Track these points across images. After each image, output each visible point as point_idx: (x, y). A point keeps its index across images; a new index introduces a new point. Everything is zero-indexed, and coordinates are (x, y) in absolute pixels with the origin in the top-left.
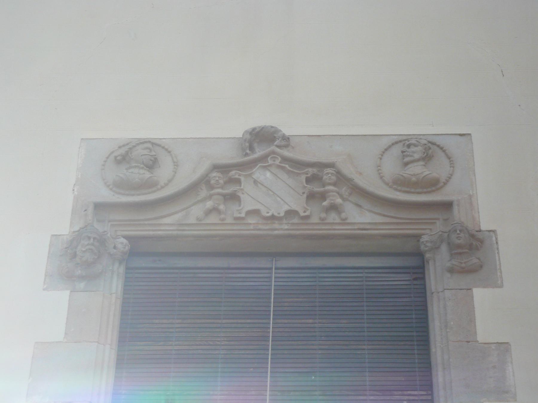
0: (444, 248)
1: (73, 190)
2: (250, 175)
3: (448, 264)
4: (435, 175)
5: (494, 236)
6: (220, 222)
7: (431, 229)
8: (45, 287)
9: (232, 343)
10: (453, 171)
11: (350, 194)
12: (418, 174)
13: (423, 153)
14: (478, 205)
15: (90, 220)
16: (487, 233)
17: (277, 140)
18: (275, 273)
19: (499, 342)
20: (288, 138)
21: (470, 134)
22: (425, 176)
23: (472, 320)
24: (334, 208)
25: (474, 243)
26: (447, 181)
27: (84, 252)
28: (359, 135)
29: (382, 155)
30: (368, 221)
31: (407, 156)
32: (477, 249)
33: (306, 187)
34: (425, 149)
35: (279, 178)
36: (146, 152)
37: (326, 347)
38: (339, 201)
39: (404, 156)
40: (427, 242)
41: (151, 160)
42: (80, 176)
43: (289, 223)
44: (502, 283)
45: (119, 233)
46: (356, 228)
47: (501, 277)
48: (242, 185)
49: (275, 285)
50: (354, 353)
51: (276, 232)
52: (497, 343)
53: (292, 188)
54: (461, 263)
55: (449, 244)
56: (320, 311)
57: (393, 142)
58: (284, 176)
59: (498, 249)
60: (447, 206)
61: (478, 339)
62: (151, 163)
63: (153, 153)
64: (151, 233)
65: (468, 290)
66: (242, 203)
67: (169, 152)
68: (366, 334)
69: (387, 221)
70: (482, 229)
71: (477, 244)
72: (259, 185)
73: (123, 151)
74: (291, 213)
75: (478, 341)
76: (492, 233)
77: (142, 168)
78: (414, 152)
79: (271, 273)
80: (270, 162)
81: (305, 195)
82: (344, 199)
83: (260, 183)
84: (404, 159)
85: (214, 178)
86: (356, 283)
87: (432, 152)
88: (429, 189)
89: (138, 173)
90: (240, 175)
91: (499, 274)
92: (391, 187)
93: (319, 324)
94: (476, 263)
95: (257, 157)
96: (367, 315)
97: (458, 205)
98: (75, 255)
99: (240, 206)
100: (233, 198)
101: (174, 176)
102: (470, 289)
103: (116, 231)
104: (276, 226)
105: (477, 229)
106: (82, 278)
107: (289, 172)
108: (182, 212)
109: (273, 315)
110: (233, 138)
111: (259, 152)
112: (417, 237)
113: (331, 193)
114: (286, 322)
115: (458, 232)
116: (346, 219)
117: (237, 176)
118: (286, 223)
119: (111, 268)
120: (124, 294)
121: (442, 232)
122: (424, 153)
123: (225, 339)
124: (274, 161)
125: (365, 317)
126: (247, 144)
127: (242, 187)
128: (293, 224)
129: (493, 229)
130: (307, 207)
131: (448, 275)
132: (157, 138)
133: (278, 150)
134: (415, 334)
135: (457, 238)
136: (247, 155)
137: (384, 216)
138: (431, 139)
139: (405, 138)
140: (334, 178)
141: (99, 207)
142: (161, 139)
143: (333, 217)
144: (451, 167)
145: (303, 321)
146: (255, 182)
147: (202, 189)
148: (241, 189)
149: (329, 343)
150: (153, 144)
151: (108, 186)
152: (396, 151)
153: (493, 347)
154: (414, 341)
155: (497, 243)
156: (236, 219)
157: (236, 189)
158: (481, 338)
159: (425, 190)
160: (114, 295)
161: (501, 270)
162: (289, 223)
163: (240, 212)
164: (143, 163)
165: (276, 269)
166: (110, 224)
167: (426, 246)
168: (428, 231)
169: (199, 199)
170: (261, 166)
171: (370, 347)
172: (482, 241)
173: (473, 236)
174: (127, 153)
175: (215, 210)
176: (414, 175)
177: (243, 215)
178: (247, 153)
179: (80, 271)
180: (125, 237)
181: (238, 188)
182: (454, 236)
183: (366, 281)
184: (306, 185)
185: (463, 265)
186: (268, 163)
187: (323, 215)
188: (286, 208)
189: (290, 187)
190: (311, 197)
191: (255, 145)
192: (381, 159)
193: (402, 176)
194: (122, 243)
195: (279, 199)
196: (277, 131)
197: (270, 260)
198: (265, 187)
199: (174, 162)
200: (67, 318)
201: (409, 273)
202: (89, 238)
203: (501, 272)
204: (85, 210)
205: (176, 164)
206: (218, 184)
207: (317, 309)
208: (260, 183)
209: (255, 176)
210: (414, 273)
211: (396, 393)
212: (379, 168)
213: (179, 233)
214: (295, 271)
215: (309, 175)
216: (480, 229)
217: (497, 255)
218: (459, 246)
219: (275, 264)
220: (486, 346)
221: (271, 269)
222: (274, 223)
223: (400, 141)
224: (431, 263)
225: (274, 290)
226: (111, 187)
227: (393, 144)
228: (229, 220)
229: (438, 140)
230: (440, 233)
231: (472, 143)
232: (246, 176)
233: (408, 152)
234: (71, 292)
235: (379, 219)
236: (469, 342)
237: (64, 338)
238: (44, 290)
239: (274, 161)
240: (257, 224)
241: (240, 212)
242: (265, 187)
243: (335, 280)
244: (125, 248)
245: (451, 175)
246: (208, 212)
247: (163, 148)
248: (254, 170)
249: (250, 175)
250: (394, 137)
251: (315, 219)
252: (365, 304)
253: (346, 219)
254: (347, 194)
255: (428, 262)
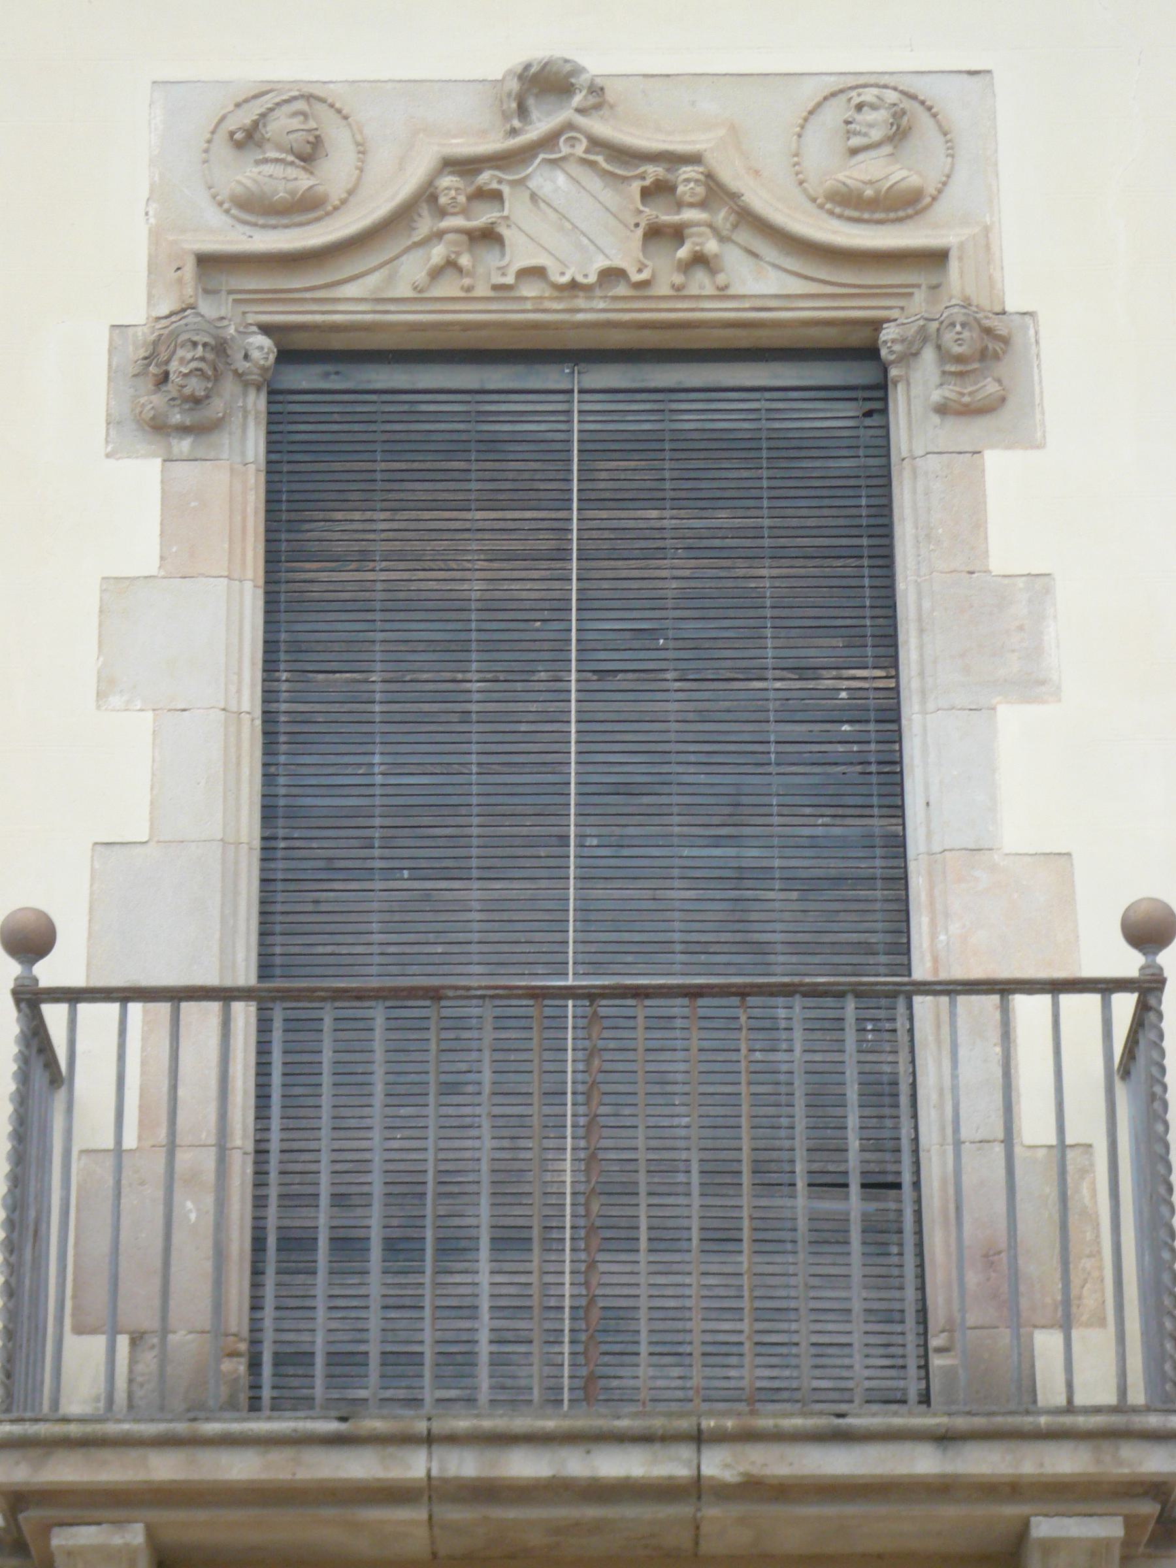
0: (929, 355)
1: (147, 214)
2: (521, 182)
3: (936, 396)
4: (914, 180)
5: (1032, 326)
6: (463, 294)
7: (902, 308)
8: (109, 449)
9: (496, 565)
10: (953, 165)
11: (735, 226)
12: (877, 181)
13: (889, 126)
14: (1001, 249)
15: (191, 297)
16: (1017, 317)
17: (577, 91)
18: (579, 402)
19: (1034, 572)
20: (602, 89)
21: (989, 72)
22: (891, 187)
23: (979, 525)
24: (700, 260)
25: (990, 346)
26: (940, 191)
27: (185, 375)
28: (752, 75)
29: (802, 127)
30: (773, 290)
31: (856, 133)
32: (997, 357)
33: (641, 212)
34: (894, 115)
35: (584, 188)
36: (296, 123)
37: (687, 573)
38: (711, 246)
39: (848, 132)
40: (894, 341)
41: (308, 142)
42: (157, 178)
43: (606, 297)
44: (1044, 436)
45: (251, 318)
46: (747, 305)
47: (1043, 424)
48: (507, 205)
49: (580, 431)
50: (820, 1370)
51: (580, 317)
52: (1029, 575)
53: (612, 213)
54: (963, 395)
55: (939, 347)
56: (674, 490)
57: (826, 92)
58: (594, 183)
59: (1038, 356)
60: (937, 258)
61: (991, 567)
62: (308, 149)
63: (312, 124)
64: (318, 318)
65: (975, 455)
66: (508, 249)
67: (346, 118)
68: (766, 542)
69: (813, 292)
70: (1007, 309)
71: (998, 349)
72: (542, 205)
73: (246, 117)
74: (611, 275)
75: (990, 572)
76: (1027, 318)
77: (292, 163)
78: (871, 125)
79: (570, 402)
80: (565, 149)
81: (640, 232)
82: (722, 239)
83: (544, 201)
84: (848, 139)
85: (446, 192)
86: (746, 425)
87: (908, 121)
88: (901, 214)
89: (284, 178)
90: (500, 181)
91: (1038, 416)
92: (821, 207)
93: (673, 521)
94: (991, 394)
95: (535, 138)
96: (769, 449)
97: (960, 259)
98: (165, 378)
99: (503, 254)
100: (488, 237)
101: (359, 179)
102: (979, 452)
103: (244, 313)
104: (581, 303)
105: (998, 309)
106: (184, 430)
107: (606, 174)
108: (382, 270)
109: (579, 500)
110: (480, 81)
111: (541, 124)
112: (876, 325)
113: (695, 230)
114: (605, 517)
115: (958, 328)
116: (726, 287)
117: (495, 185)
118: (601, 297)
119: (240, 404)
120: (269, 452)
121: (926, 319)
122: (892, 124)
123: (482, 557)
124: (573, 146)
125: (765, 503)
126: (514, 105)
127: (506, 213)
128: (615, 298)
129: (1030, 310)
130: (646, 262)
131: (936, 419)
132: (316, 82)
133: (581, 120)
134: (865, 541)
135: (956, 341)
136: (514, 132)
137: (806, 278)
138: (905, 84)
139: (852, 81)
140: (701, 190)
141: (208, 262)
142: (325, 83)
143: (701, 282)
144: (947, 156)
145: (640, 514)
146: (534, 197)
147: (420, 216)
148: (507, 218)
149: (693, 563)
150: (309, 98)
151: (221, 204)
152: (835, 113)
153: (1021, 583)
154: (862, 557)
155: (1037, 342)
156: (496, 287)
157: (494, 220)
158: (997, 564)
159: (892, 215)
160: (252, 467)
161: (1042, 407)
162: (606, 297)
163: (503, 271)
164: (291, 151)
165: (580, 392)
166: (232, 297)
167: (892, 352)
168: (894, 314)
169: (416, 239)
170: (544, 160)
171: (775, 572)
172: (1005, 341)
173: (988, 331)
174: (256, 124)
175: (451, 264)
176: (871, 183)
177: (510, 280)
178: (514, 129)
179: (178, 416)
180: (266, 329)
181: (498, 214)
182: (948, 337)
183: (768, 419)
184: (642, 208)
185: (966, 399)
186: (560, 152)
187: (678, 279)
188: (601, 263)
189: (607, 209)
190: (654, 233)
191: (531, 102)
192: (799, 136)
193: (844, 184)
194: (261, 348)
195: (585, 241)
196: (577, 70)
197: (567, 371)
198: (556, 210)
199: (358, 144)
200: (162, 524)
201: (856, 399)
202: (195, 344)
203: (1043, 413)
204: (179, 269)
205: (362, 150)
206: (454, 207)
207: (668, 485)
208: (544, 201)
209: (532, 184)
210: (864, 399)
211: (825, 673)
212: (797, 167)
213: (378, 317)
214: (621, 396)
215: (647, 183)
216: (1004, 309)
217: (1036, 370)
218: (959, 359)
219: (578, 382)
220: (1006, 581)
221: (572, 391)
222: (576, 297)
223: (842, 91)
224: (901, 387)
225: (579, 441)
226: (226, 206)
227: (826, 99)
228: (482, 290)
229: (919, 86)
230: (922, 322)
231: (994, 95)
232: (513, 184)
233: (859, 124)
234: (165, 461)
235: (796, 286)
236: (972, 573)
237: (160, 567)
238: (108, 456)
239: (573, 146)
240: (541, 298)
241: (503, 271)
242: (556, 210)
243: (703, 417)
244: (267, 359)
245: (948, 176)
246: (436, 274)
247: (332, 106)
248: (530, 169)
249: (521, 182)
250: (827, 78)
251: (662, 289)
252: (765, 473)
253: (726, 287)
254: (728, 226)
255: (895, 384)
